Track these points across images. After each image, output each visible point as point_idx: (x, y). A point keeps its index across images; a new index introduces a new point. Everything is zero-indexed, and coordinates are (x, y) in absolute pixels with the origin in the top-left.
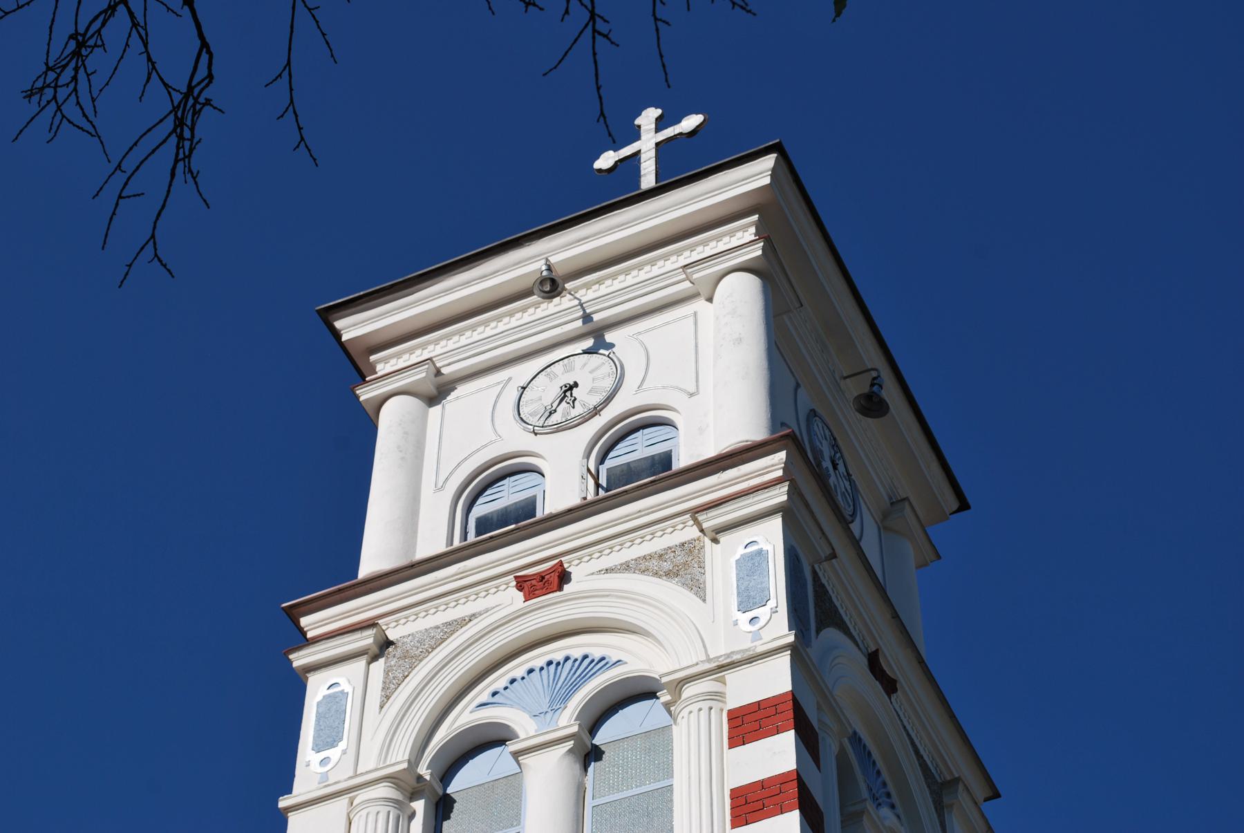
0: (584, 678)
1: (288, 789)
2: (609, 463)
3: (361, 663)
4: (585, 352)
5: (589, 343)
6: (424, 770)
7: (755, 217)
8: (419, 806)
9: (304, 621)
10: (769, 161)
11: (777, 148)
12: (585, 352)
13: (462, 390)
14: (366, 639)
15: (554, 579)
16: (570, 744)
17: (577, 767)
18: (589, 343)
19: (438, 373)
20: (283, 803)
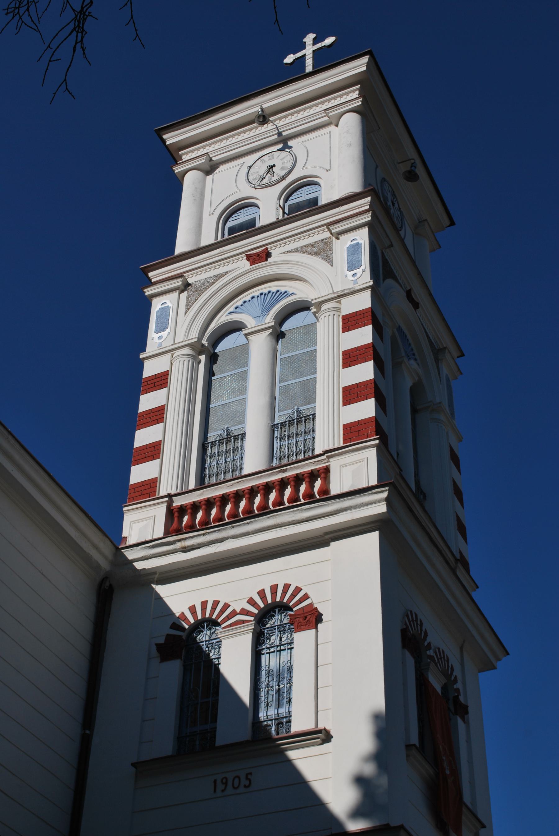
2: (289, 202)
3: (176, 294)
5: (281, 146)
6: (205, 342)
8: (203, 358)
9: (150, 274)
12: (279, 150)
13: (222, 168)
14: (178, 283)
16: (270, 331)
19: (211, 160)
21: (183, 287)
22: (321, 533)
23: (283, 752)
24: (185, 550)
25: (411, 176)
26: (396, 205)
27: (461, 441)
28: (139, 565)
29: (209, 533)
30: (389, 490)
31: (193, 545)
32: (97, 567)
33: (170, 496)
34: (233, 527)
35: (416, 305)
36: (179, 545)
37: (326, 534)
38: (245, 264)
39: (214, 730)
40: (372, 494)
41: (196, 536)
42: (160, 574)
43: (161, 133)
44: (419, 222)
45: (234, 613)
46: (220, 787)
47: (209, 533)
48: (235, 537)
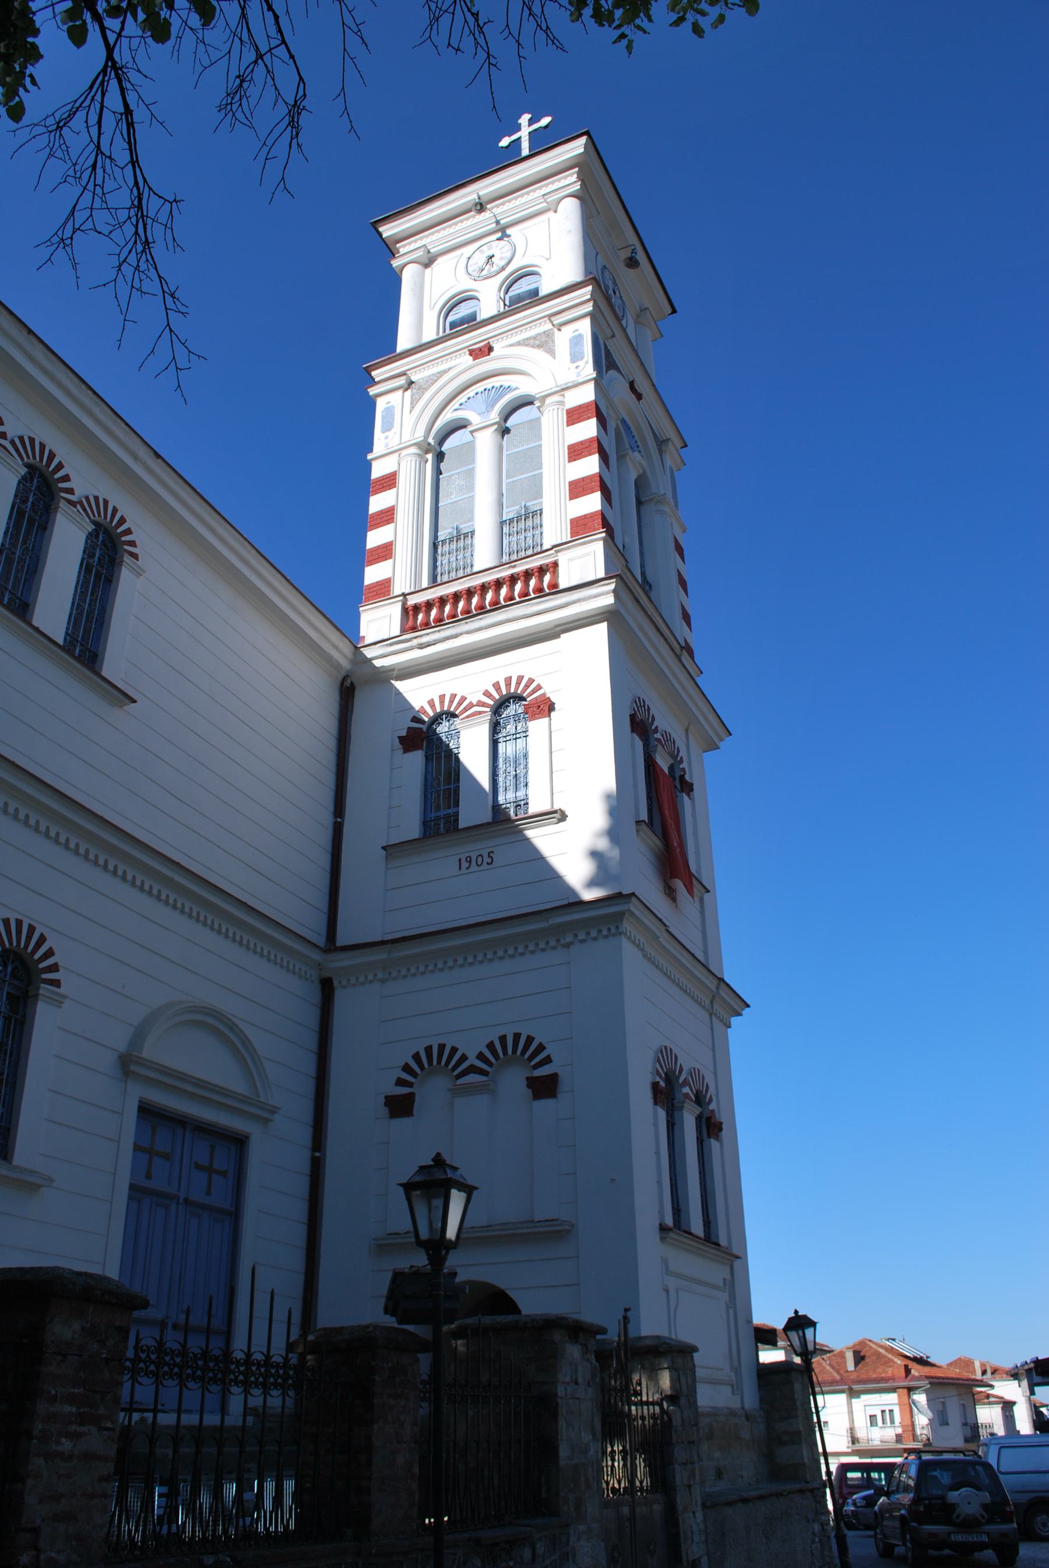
0: (501, 396)
2: (510, 294)
5: (499, 235)
7: (577, 169)
8: (430, 456)
9: (373, 373)
10: (583, 140)
11: (587, 133)
12: (498, 239)
13: (440, 260)
16: (496, 427)
17: (499, 437)
18: (499, 235)
19: (429, 252)
20: (369, 457)
22: (552, 626)
23: (521, 831)
24: (421, 647)
25: (632, 263)
26: (617, 293)
27: (685, 532)
28: (377, 663)
32: (337, 666)
33: (404, 595)
34: (467, 623)
35: (639, 397)
36: (415, 642)
37: (556, 626)
38: (468, 360)
39: (457, 814)
42: (399, 670)
43: (377, 226)
44: (641, 311)
45: (471, 705)
46: (465, 865)
48: (468, 632)
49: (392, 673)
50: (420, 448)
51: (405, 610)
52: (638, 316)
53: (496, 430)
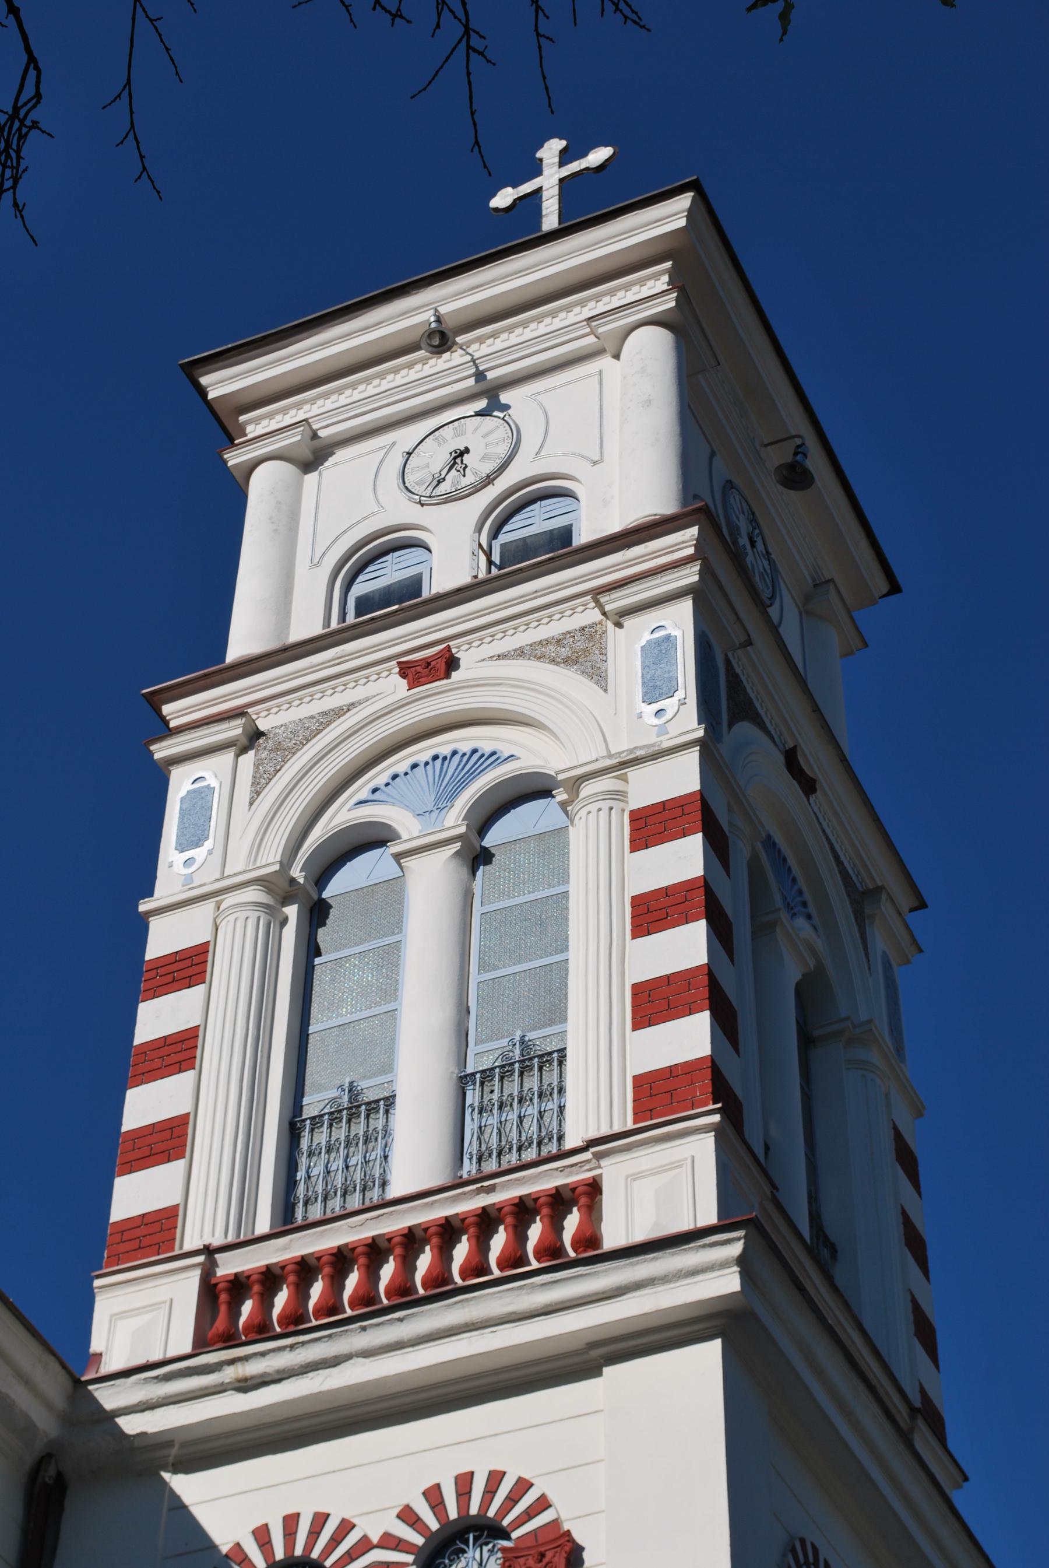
1: (149, 892)
2: (503, 538)
3: (228, 756)
4: (478, 414)
5: (482, 404)
6: (297, 872)
8: (292, 911)
9: (167, 709)
10: (684, 201)
12: (478, 414)
13: (341, 455)
14: (234, 730)
15: (442, 665)
17: (465, 872)
19: (315, 436)
21: (244, 741)
24: (245, 1386)
28: (130, 1425)
29: (303, 1343)
30: (745, 1237)
31: (265, 1374)
33: (209, 1251)
34: (364, 1329)
35: (809, 786)
36: (229, 1374)
38: (396, 686)
40: (704, 1246)
41: (273, 1350)
44: (816, 586)
47: (303, 1343)
48: (367, 1353)
49: (165, 1452)
50: (269, 891)
51: (209, 1290)
52: (808, 599)
53: (457, 853)
